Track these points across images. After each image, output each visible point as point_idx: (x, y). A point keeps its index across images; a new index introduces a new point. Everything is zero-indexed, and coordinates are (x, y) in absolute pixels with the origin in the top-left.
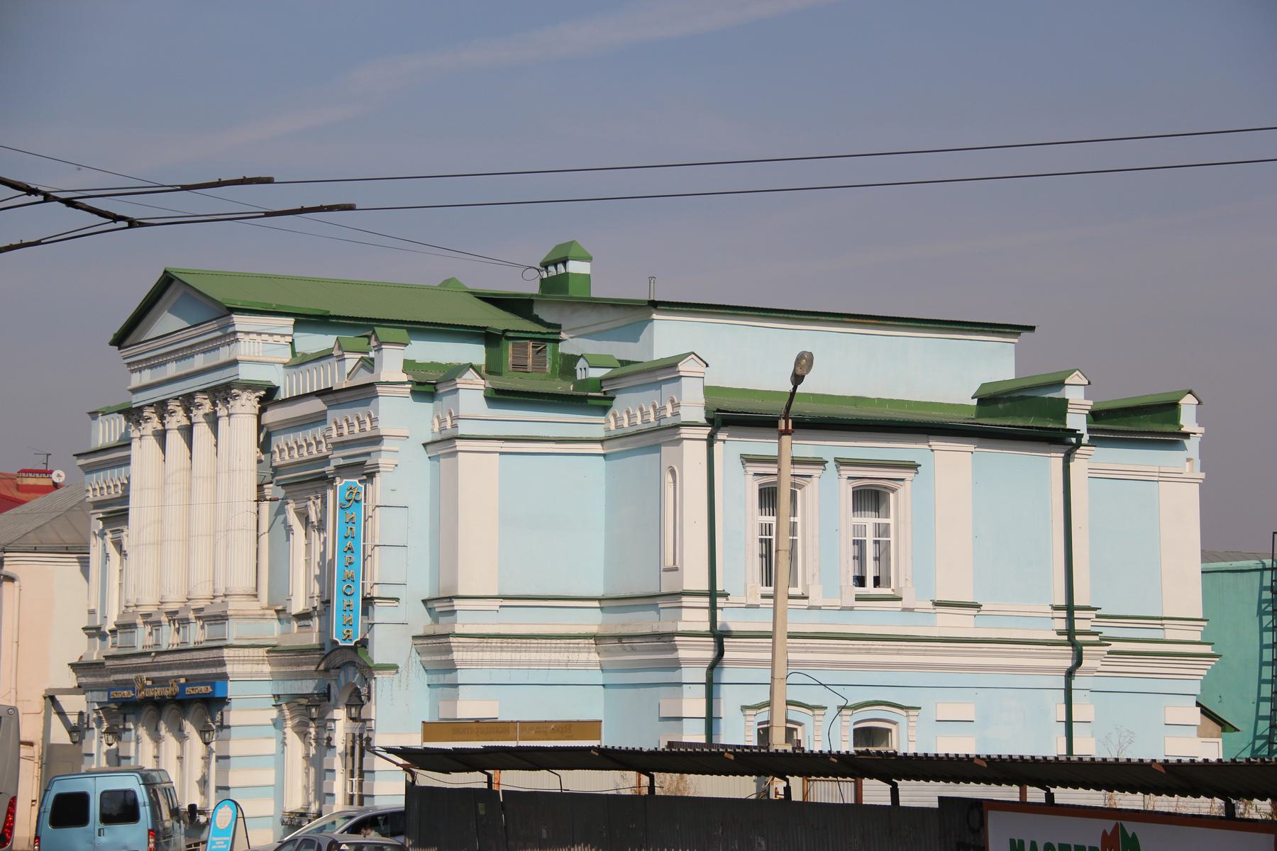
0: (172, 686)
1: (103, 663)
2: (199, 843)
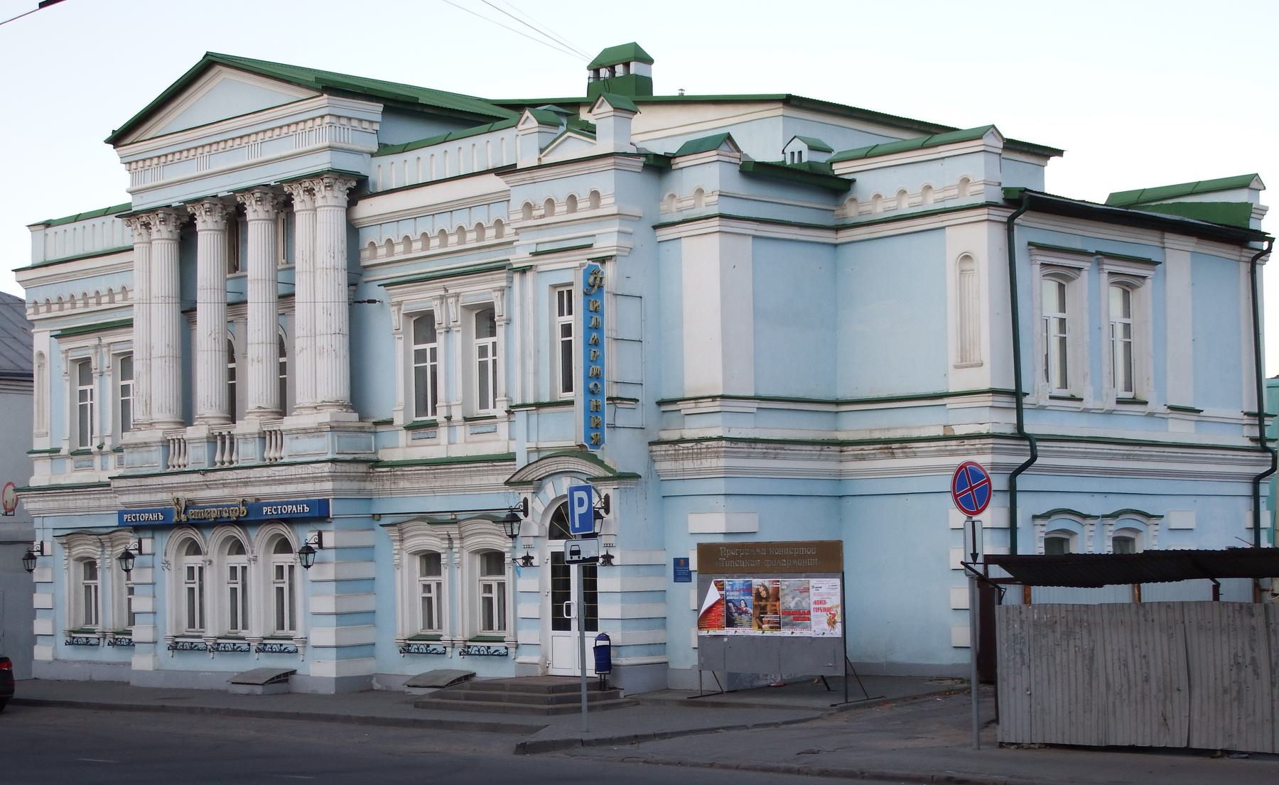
1: (109, 485)
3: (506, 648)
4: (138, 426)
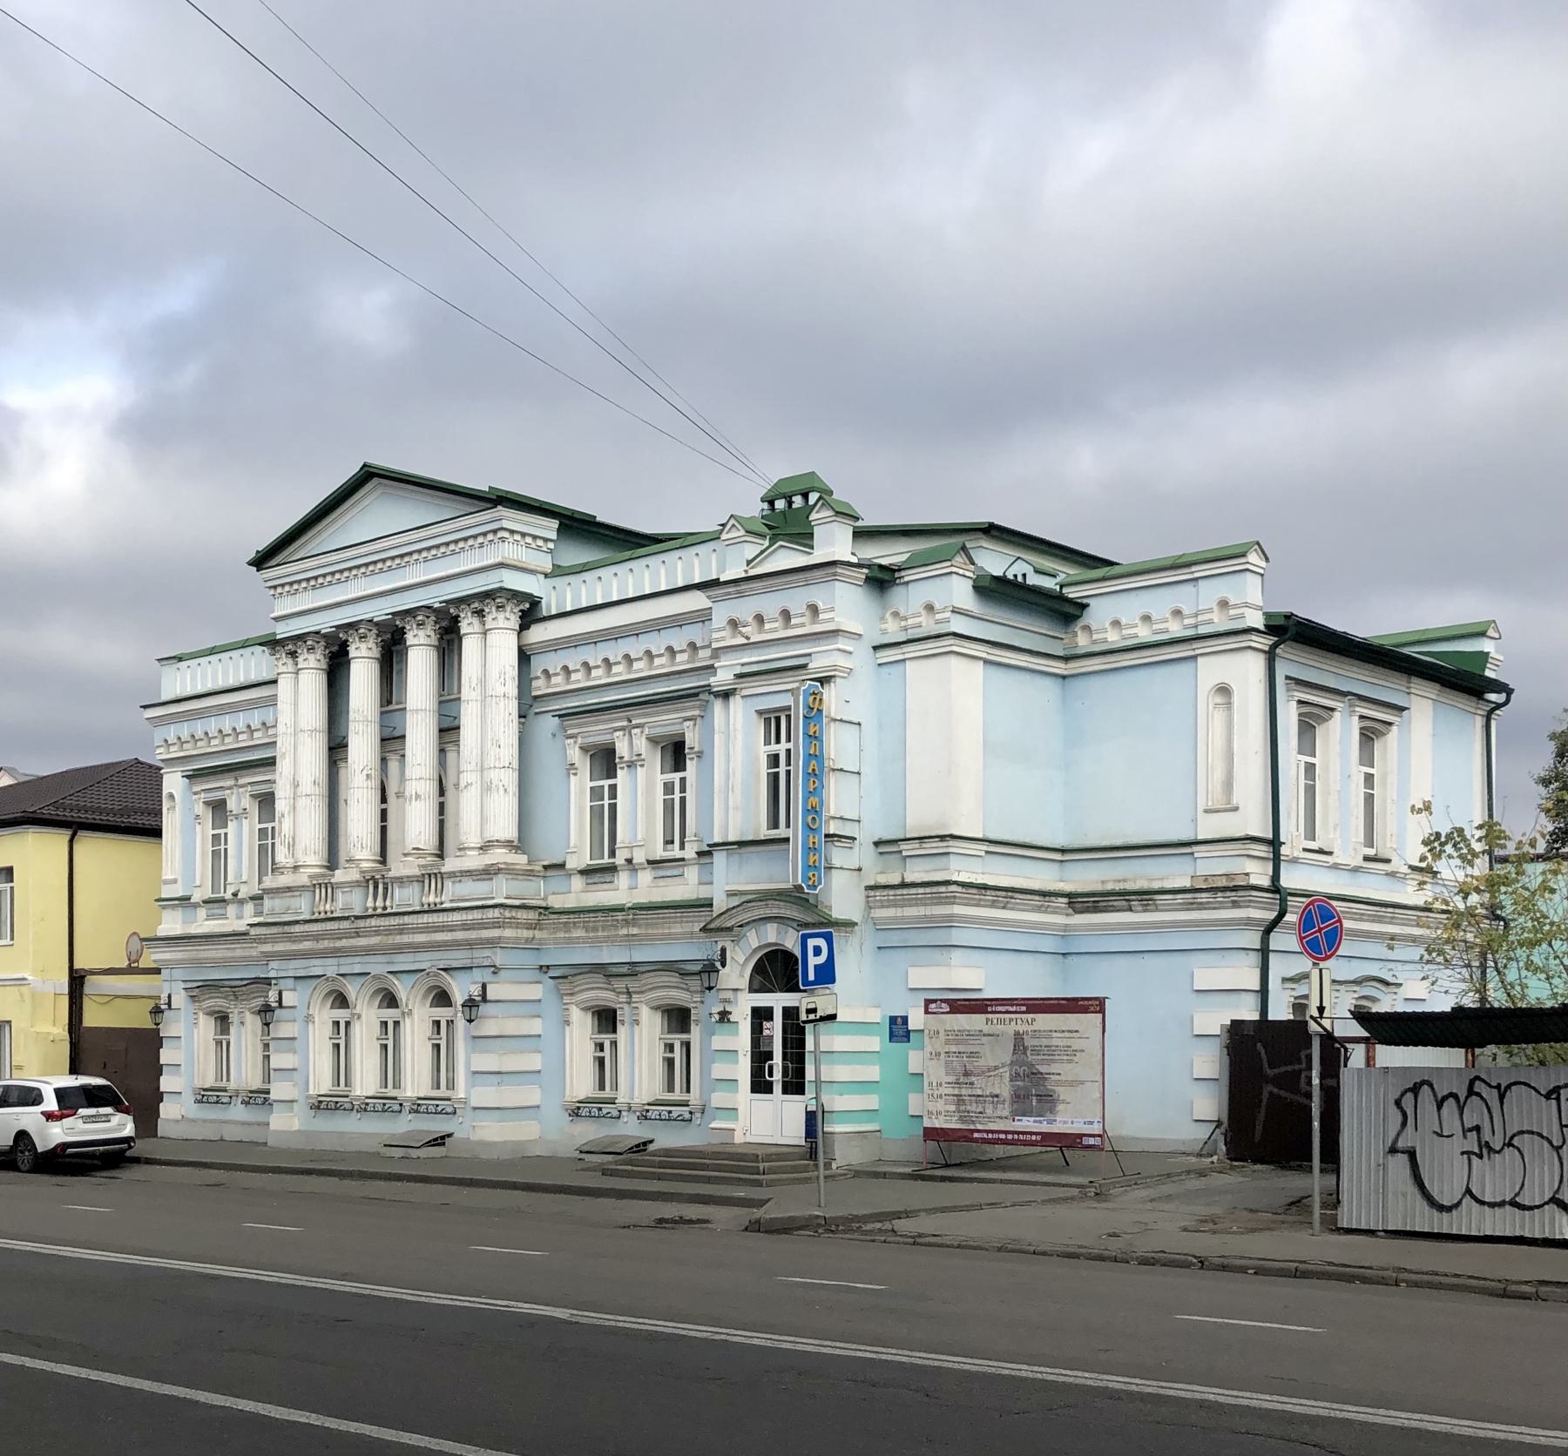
3: (691, 1113)
4: (281, 870)
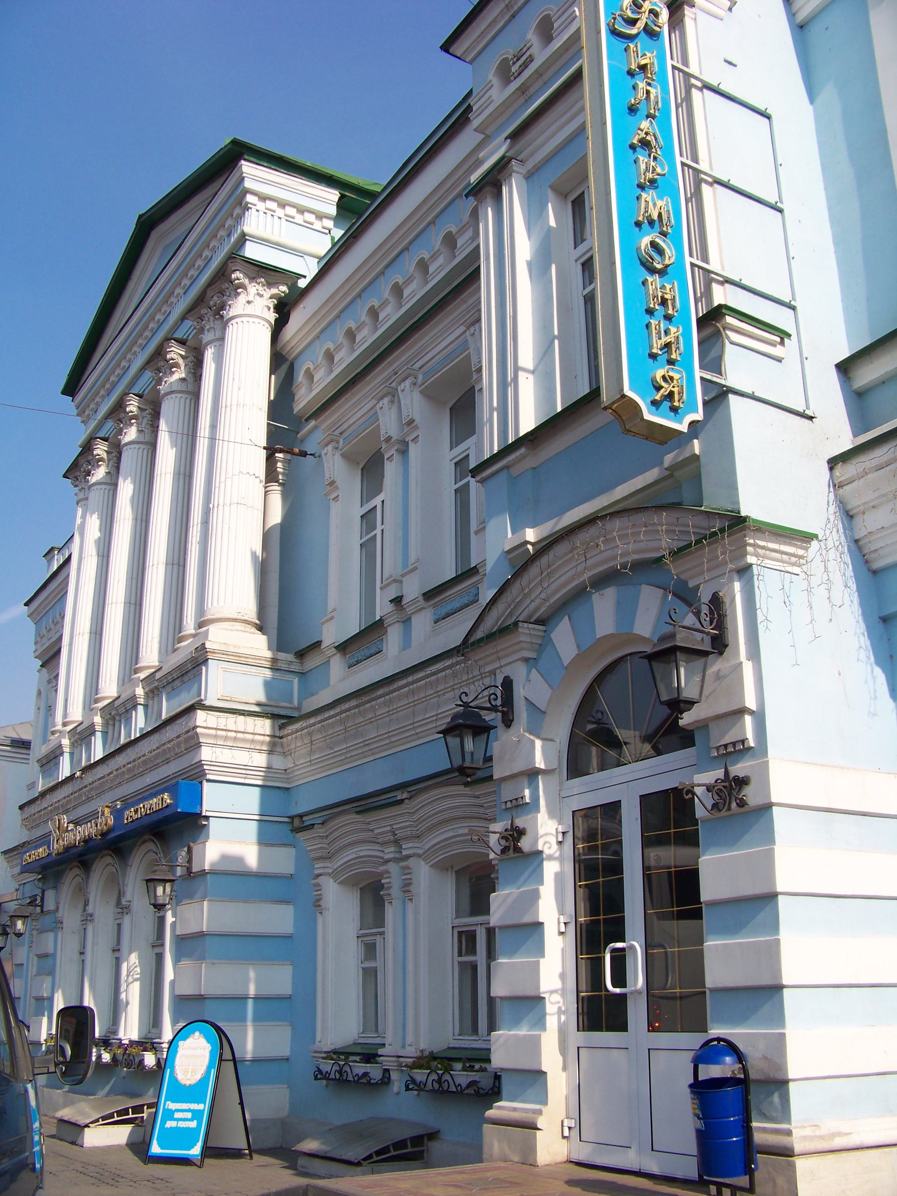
0: (103, 814)
2: (143, 1105)
